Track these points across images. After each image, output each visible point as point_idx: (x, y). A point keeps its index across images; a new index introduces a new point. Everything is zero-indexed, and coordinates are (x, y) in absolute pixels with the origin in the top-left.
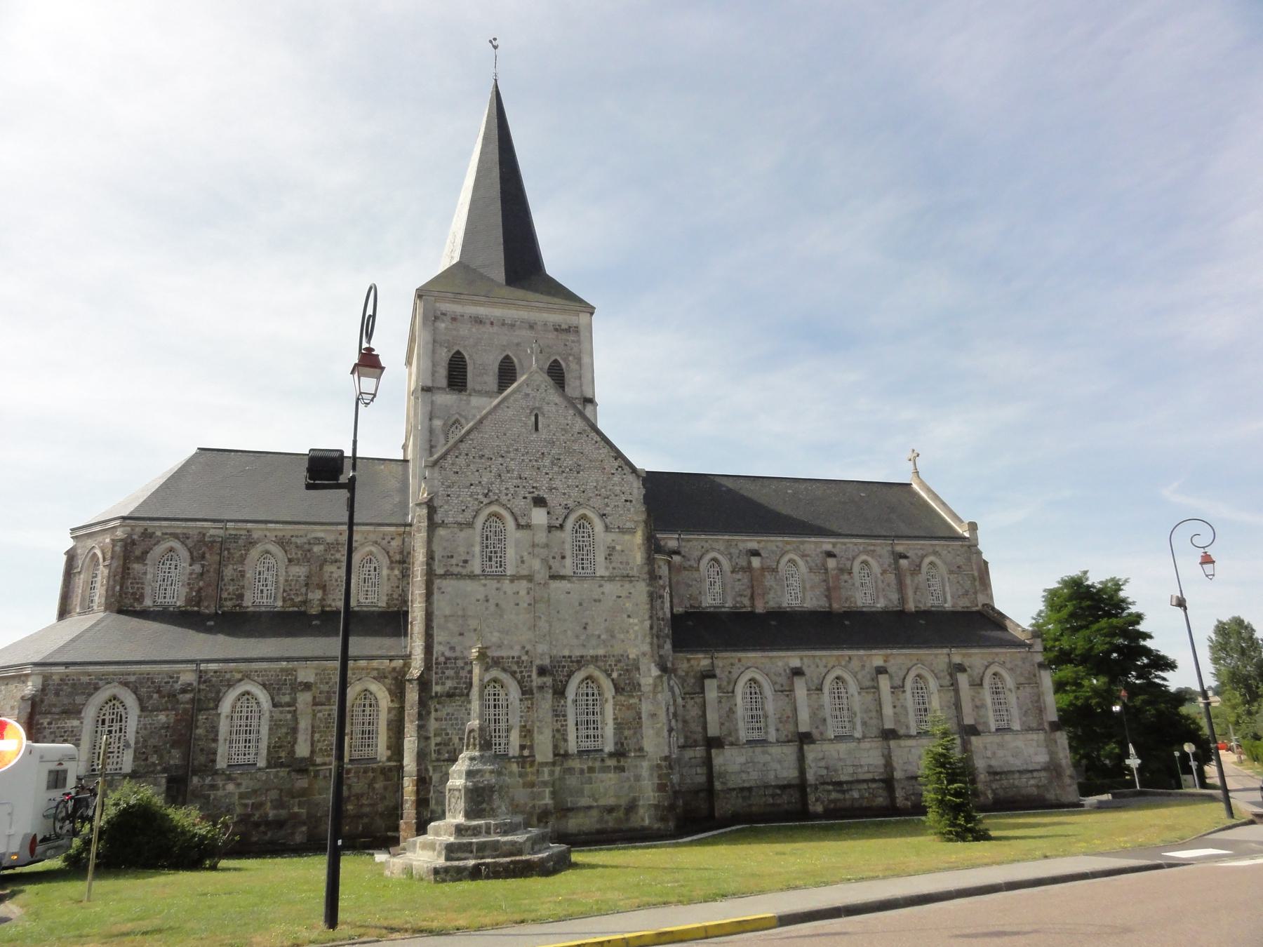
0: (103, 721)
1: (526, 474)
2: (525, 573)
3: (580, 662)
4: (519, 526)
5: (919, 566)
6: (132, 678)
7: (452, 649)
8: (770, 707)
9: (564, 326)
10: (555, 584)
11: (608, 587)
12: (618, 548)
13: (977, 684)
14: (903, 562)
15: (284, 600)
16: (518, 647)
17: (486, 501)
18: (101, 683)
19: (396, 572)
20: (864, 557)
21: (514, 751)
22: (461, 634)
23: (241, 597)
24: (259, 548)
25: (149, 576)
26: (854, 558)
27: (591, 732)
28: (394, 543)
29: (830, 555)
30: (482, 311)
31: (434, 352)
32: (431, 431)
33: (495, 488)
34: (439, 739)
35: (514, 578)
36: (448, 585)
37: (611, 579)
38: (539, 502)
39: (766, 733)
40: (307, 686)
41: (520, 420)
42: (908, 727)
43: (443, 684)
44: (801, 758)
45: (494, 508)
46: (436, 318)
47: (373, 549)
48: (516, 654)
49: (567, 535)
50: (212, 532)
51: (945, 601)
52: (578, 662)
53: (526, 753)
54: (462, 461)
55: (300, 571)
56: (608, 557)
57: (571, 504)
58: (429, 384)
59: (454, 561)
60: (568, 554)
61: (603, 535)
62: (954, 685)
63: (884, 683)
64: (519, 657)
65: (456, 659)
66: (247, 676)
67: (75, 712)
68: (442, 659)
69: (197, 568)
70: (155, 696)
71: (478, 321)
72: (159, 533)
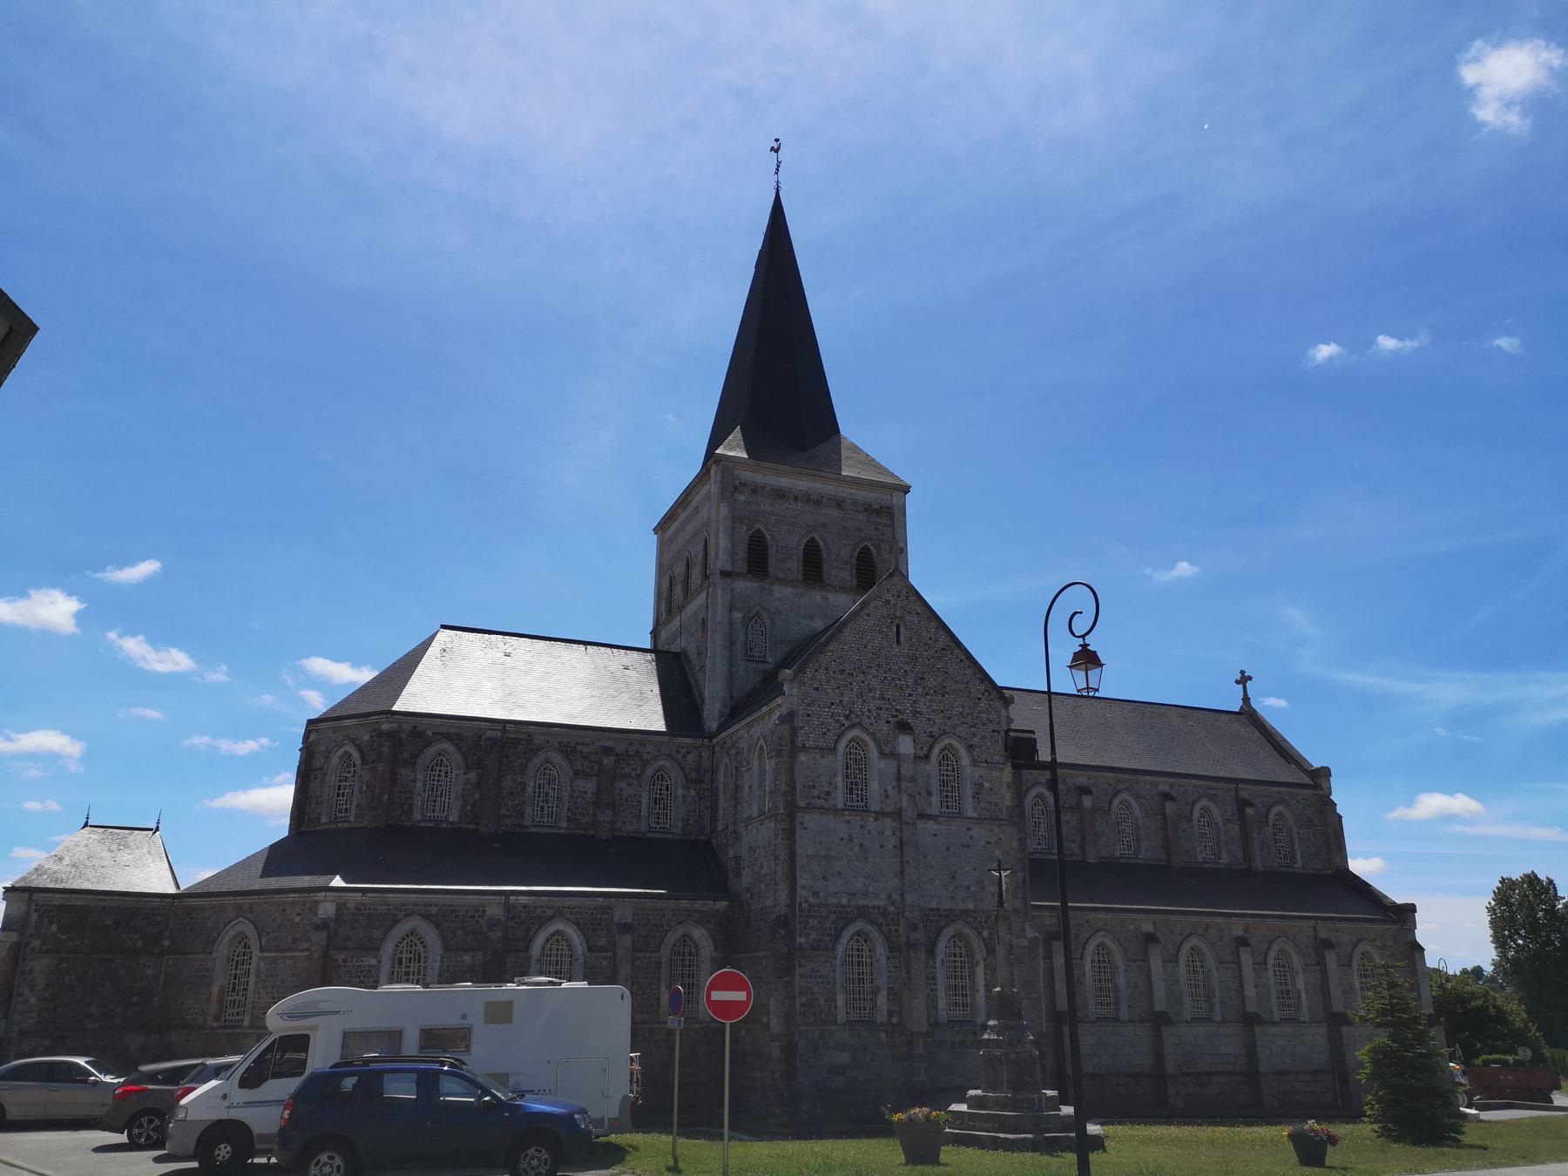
0: (400, 960)
1: (889, 694)
2: (890, 809)
3: (950, 916)
4: (882, 754)
5: (1266, 816)
6: (434, 910)
7: (816, 894)
8: (1122, 980)
9: (875, 506)
10: (921, 825)
11: (976, 831)
12: (986, 785)
13: (1346, 963)
14: (1249, 811)
15: (569, 820)
16: (884, 896)
17: (847, 723)
18: (400, 915)
19: (693, 793)
20: (1204, 802)
21: (881, 1017)
22: (825, 878)
23: (521, 814)
24: (542, 756)
25: (419, 785)
26: (1194, 804)
27: (960, 999)
28: (690, 758)
29: (1167, 797)
30: (784, 482)
31: (733, 529)
32: (731, 624)
33: (856, 709)
34: (804, 999)
35: (881, 814)
36: (811, 820)
37: (979, 820)
38: (904, 727)
39: (1117, 1009)
40: (625, 928)
41: (881, 631)
42: (1271, 1012)
43: (807, 934)
44: (1158, 1041)
45: (856, 732)
46: (736, 488)
47: (667, 763)
48: (882, 904)
49: (932, 767)
50: (489, 734)
51: (1294, 861)
52: (947, 916)
53: (895, 1020)
54: (821, 676)
55: (589, 786)
56: (976, 796)
57: (935, 730)
58: (729, 568)
59: (816, 793)
60: (935, 789)
61: (969, 770)
62: (1321, 963)
63: (1246, 958)
64: (885, 908)
65: (820, 906)
66: (559, 914)
67: (373, 948)
68: (805, 906)
69: (472, 776)
70: (459, 932)
71: (781, 494)
72: (429, 733)
